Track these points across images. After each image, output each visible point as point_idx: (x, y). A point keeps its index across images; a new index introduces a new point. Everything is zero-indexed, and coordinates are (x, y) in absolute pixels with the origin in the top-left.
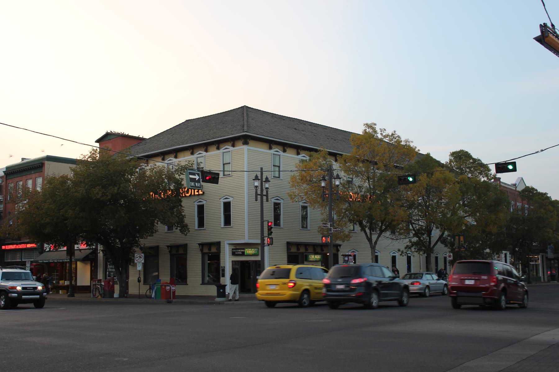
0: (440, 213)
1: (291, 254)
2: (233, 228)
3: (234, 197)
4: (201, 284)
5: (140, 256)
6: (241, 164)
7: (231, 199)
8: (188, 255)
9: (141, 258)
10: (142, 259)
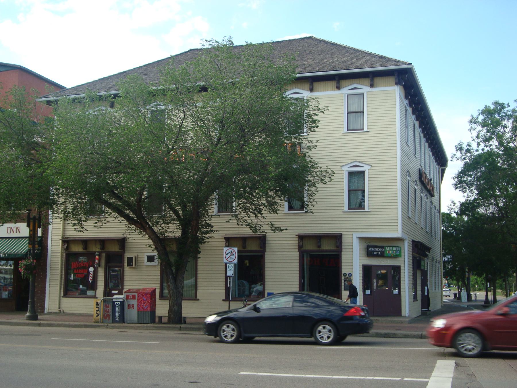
0: (120, 179)
1: (243, 254)
2: (371, 213)
3: (373, 165)
4: (223, 300)
5: (231, 251)
6: (392, 115)
7: (366, 168)
8: (266, 253)
9: (233, 255)
10: (234, 257)
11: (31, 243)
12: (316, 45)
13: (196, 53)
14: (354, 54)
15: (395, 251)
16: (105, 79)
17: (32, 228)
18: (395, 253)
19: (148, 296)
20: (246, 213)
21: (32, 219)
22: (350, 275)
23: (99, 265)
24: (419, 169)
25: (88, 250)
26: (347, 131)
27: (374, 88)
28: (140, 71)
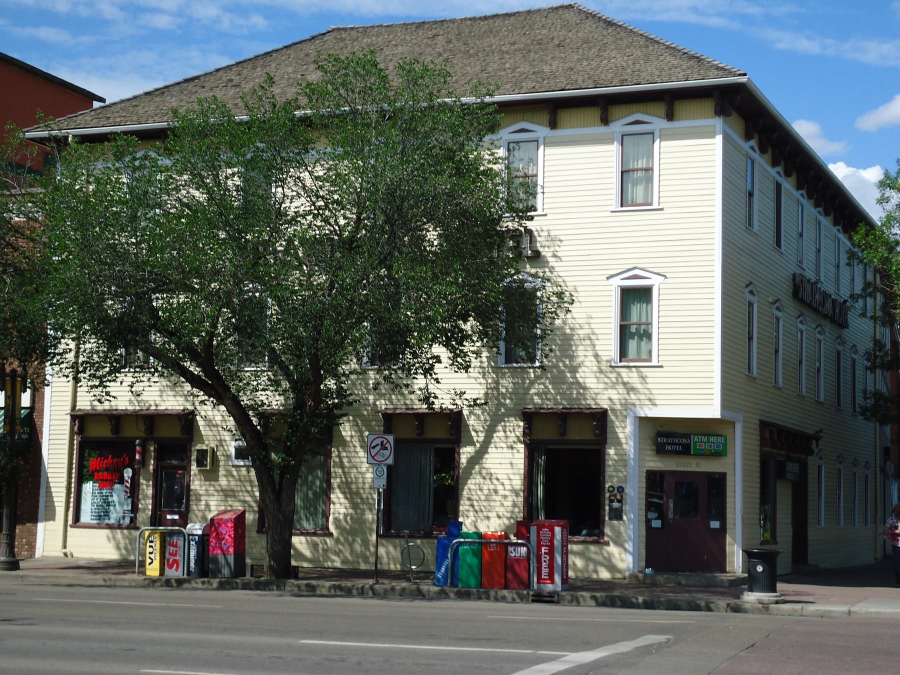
5: (382, 442)
7: (654, 281)
9: (386, 449)
10: (387, 453)
11: (7, 421)
12: (578, 24)
13: (341, 38)
14: (644, 49)
15: (714, 443)
16: (157, 93)
17: (9, 394)
18: (714, 448)
19: (229, 525)
20: (348, 393)
21: (8, 375)
22: (620, 490)
23: (144, 463)
24: (794, 275)
25: (121, 435)
26: (622, 206)
27: (674, 122)
28: (227, 76)
